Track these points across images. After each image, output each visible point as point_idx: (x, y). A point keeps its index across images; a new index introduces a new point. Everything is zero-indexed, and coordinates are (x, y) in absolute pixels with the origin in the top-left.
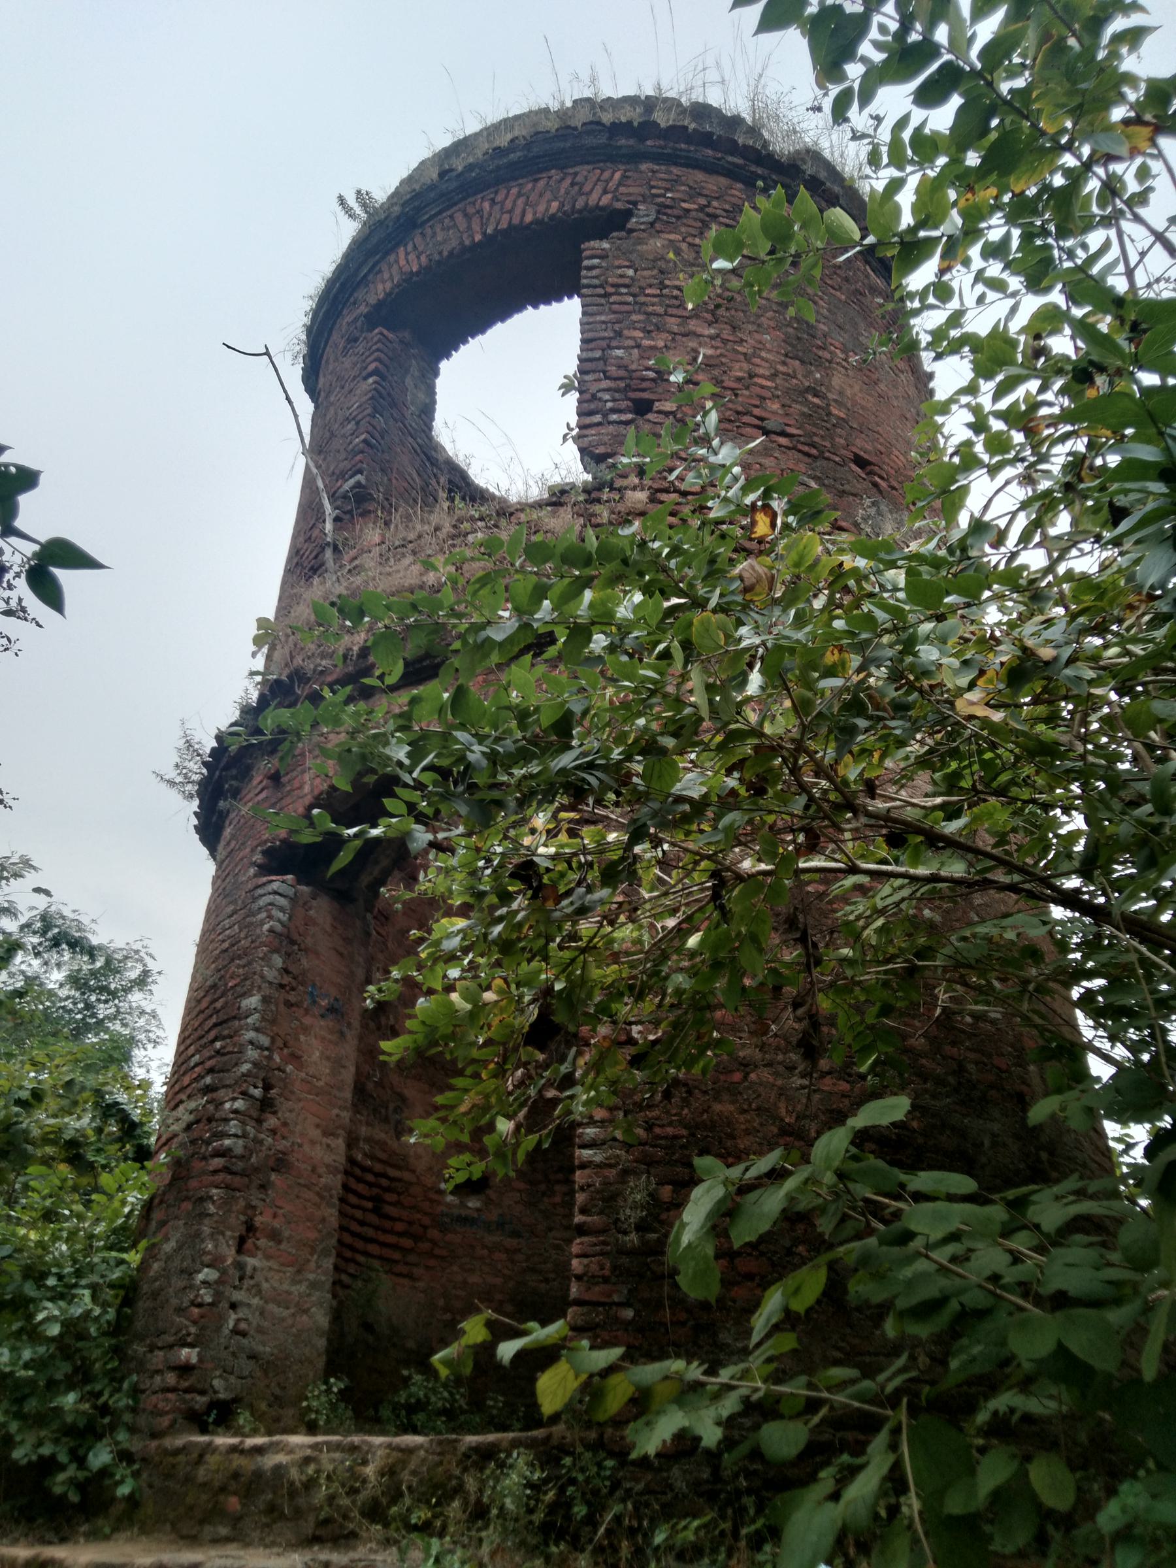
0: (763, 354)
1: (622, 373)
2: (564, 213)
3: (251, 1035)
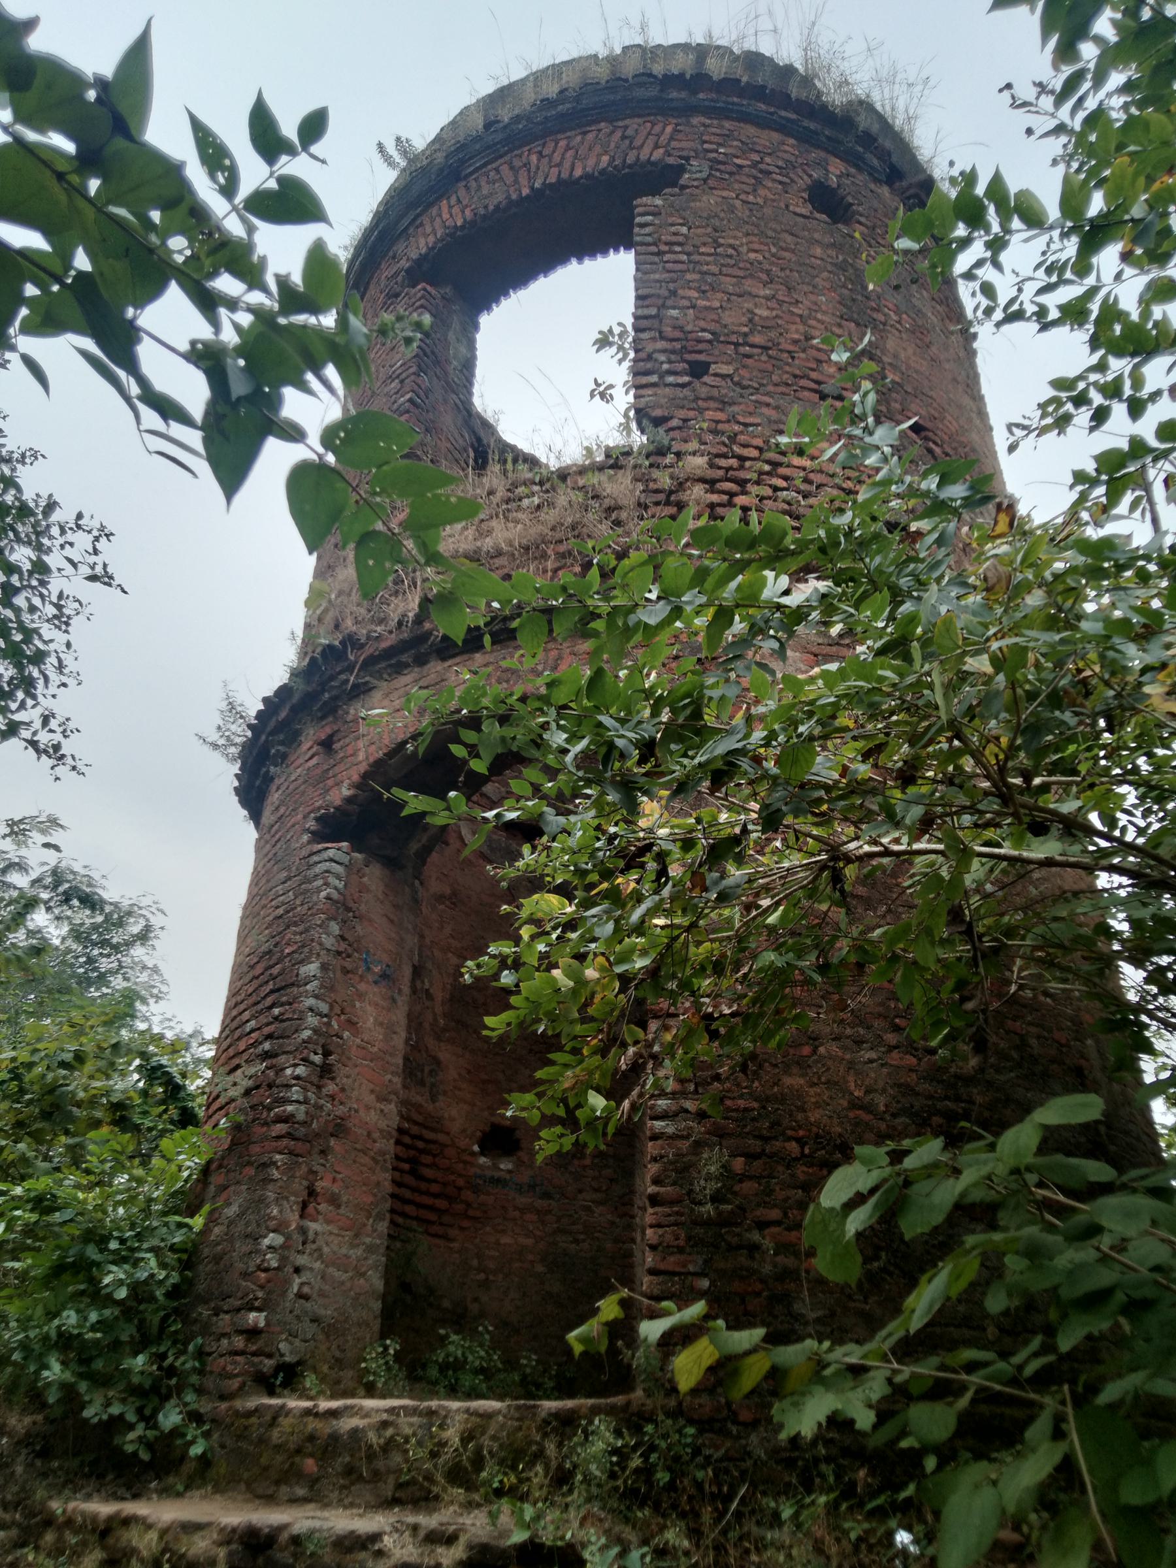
0: (819, 316)
1: (677, 334)
2: (615, 167)
3: (311, 1002)
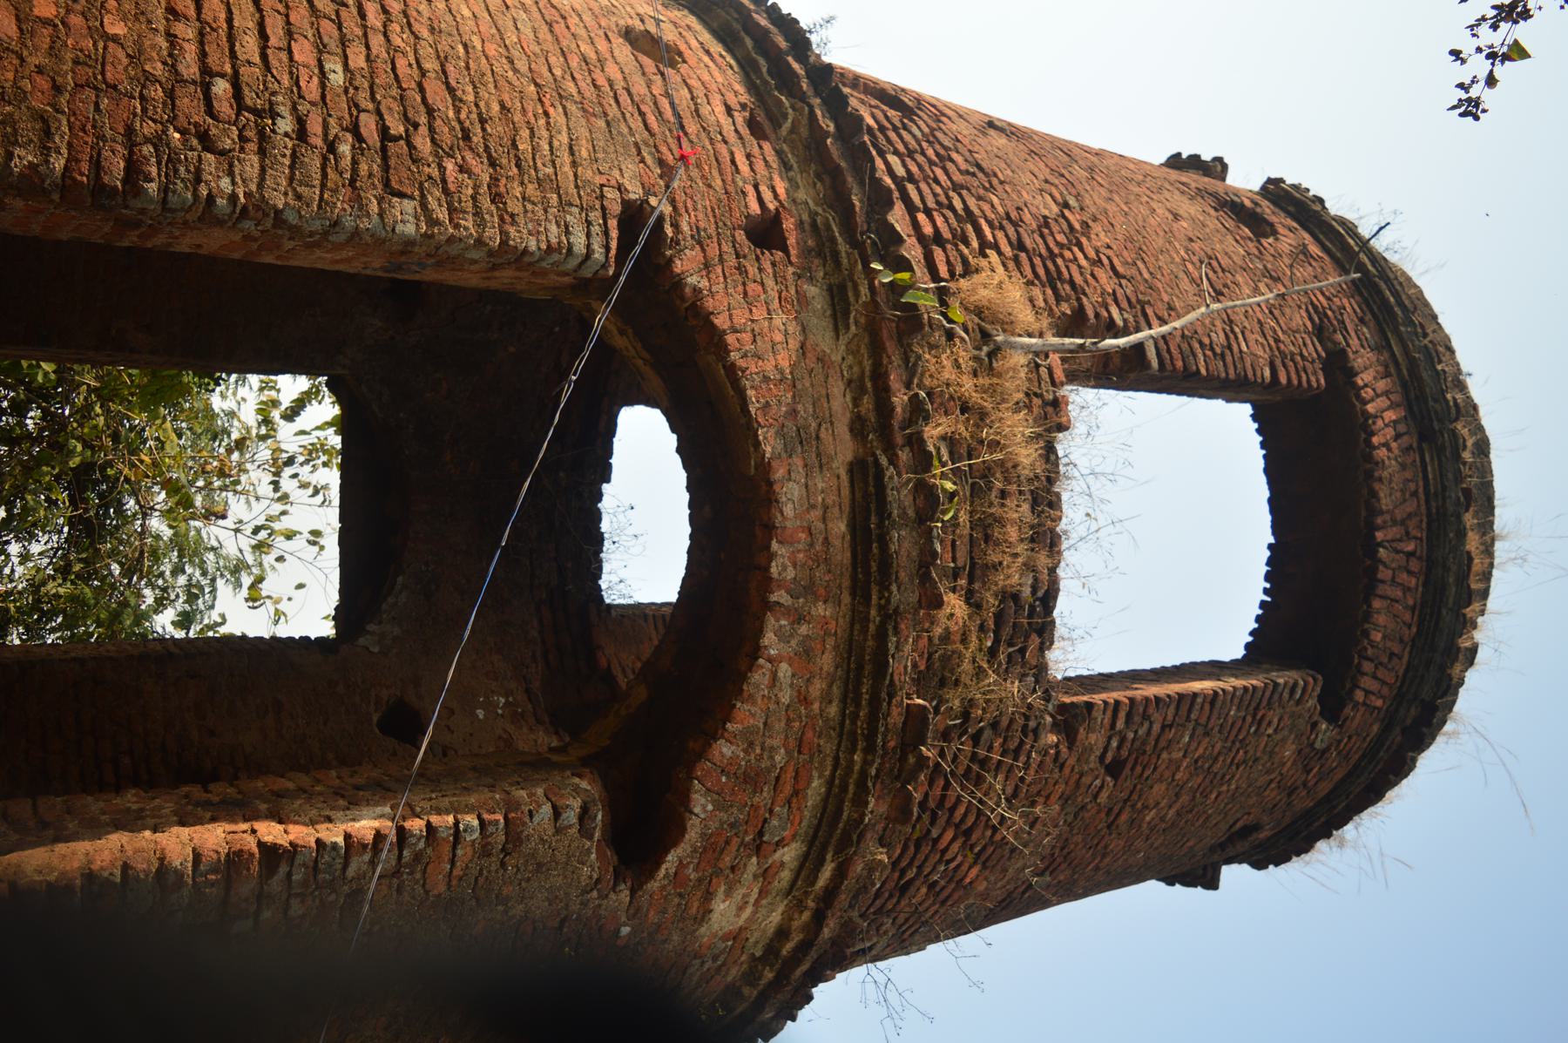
1: (1162, 744)
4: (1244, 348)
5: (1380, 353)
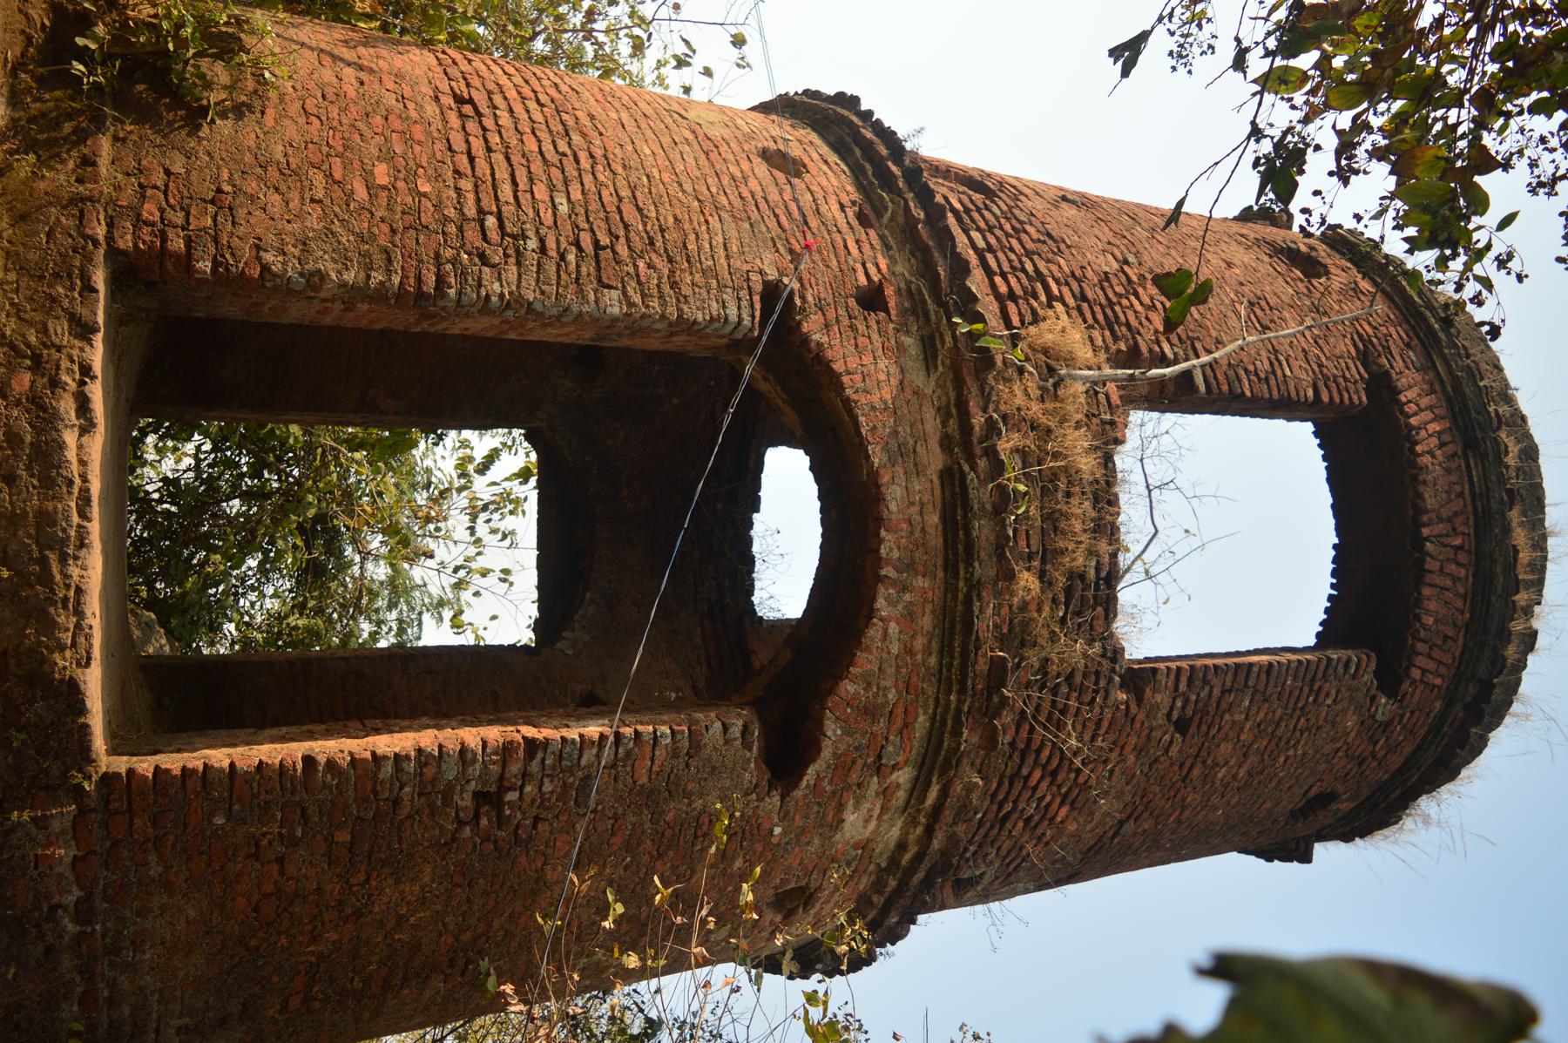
1: (1224, 706)
4: (1288, 372)
5: (1426, 373)
